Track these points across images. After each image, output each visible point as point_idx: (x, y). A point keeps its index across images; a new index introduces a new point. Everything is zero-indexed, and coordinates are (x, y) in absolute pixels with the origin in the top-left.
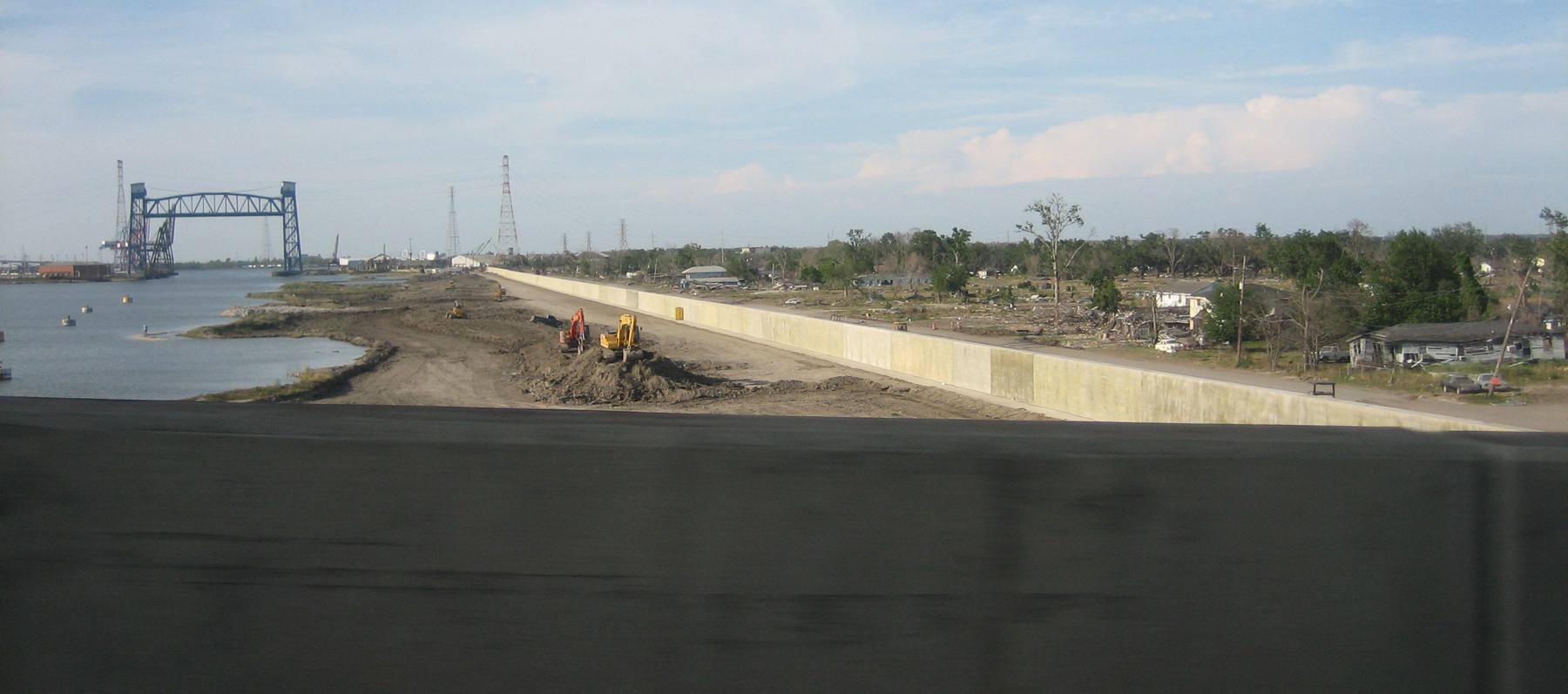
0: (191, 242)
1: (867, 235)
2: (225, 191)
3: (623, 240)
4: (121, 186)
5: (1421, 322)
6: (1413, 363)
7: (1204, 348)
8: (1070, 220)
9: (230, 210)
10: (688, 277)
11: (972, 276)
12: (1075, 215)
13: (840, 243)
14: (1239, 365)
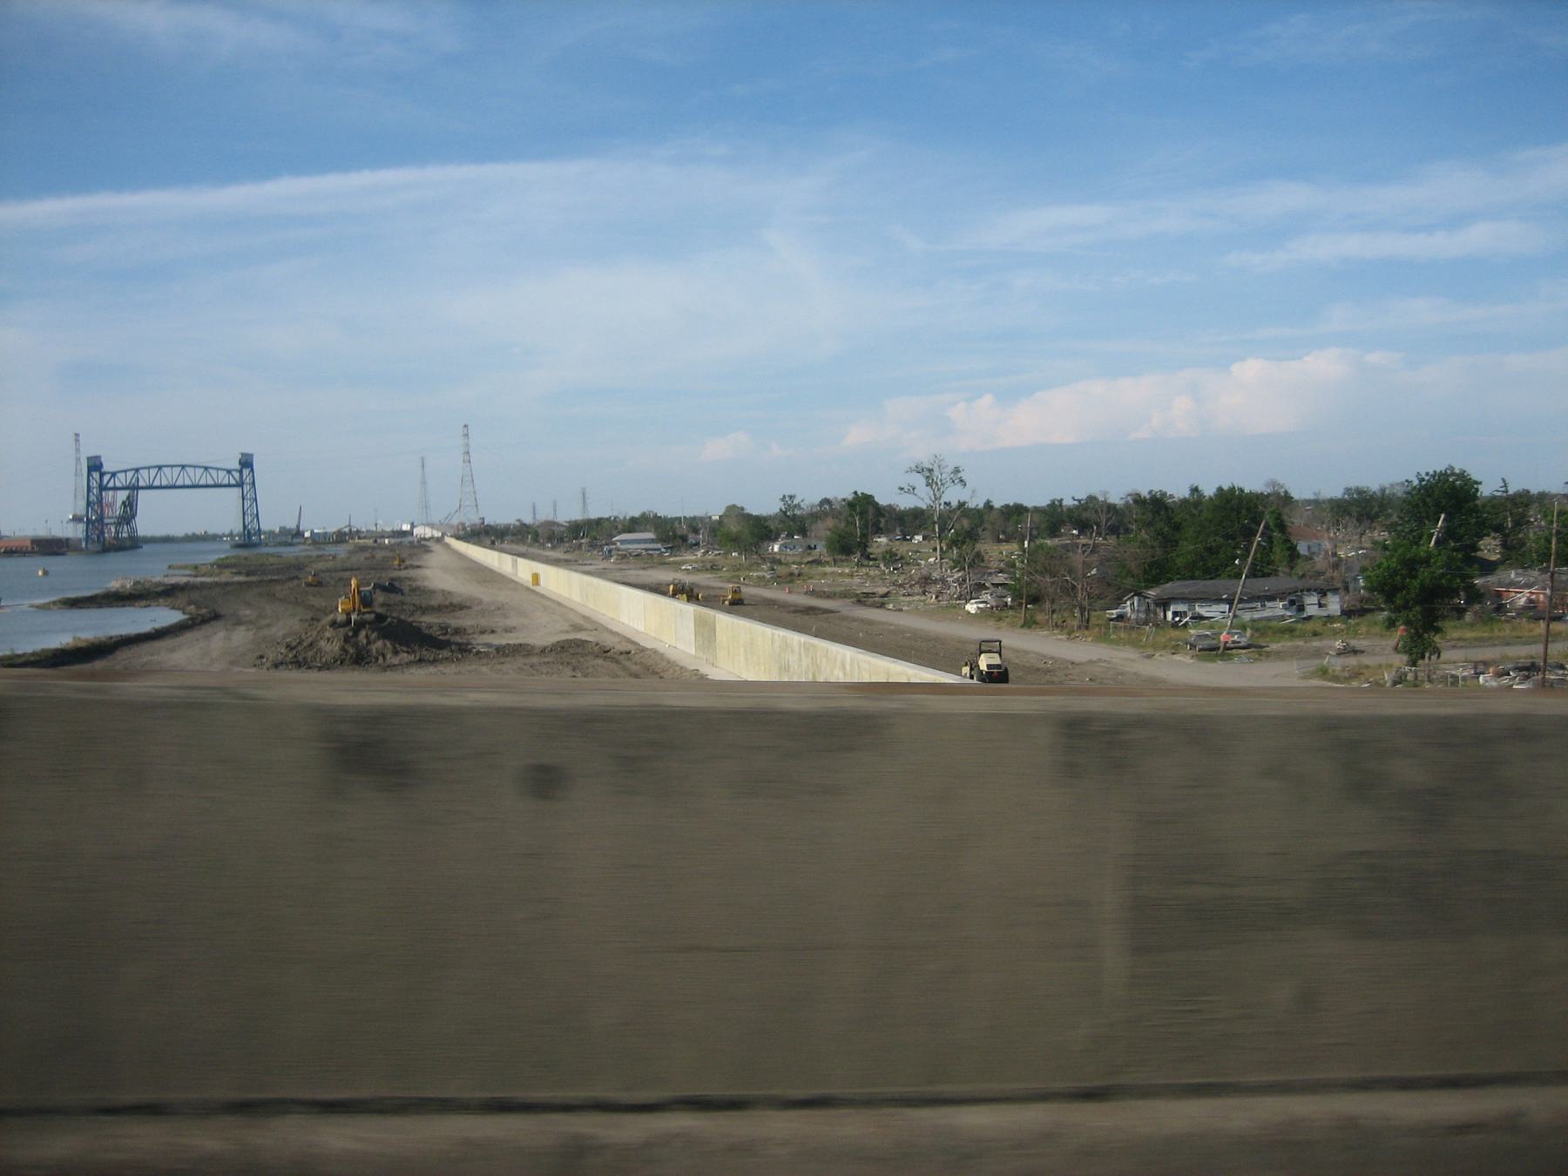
0: (155, 516)
1: (800, 500)
2: (184, 463)
3: (534, 517)
4: (78, 460)
5: (1231, 578)
6: (1180, 621)
7: (1011, 608)
8: (953, 481)
9: (210, 482)
10: (618, 544)
11: (908, 540)
12: (958, 477)
13: (738, 508)
14: (1022, 627)
